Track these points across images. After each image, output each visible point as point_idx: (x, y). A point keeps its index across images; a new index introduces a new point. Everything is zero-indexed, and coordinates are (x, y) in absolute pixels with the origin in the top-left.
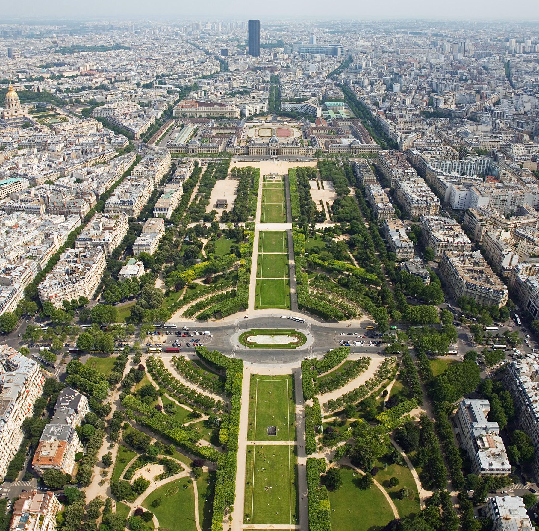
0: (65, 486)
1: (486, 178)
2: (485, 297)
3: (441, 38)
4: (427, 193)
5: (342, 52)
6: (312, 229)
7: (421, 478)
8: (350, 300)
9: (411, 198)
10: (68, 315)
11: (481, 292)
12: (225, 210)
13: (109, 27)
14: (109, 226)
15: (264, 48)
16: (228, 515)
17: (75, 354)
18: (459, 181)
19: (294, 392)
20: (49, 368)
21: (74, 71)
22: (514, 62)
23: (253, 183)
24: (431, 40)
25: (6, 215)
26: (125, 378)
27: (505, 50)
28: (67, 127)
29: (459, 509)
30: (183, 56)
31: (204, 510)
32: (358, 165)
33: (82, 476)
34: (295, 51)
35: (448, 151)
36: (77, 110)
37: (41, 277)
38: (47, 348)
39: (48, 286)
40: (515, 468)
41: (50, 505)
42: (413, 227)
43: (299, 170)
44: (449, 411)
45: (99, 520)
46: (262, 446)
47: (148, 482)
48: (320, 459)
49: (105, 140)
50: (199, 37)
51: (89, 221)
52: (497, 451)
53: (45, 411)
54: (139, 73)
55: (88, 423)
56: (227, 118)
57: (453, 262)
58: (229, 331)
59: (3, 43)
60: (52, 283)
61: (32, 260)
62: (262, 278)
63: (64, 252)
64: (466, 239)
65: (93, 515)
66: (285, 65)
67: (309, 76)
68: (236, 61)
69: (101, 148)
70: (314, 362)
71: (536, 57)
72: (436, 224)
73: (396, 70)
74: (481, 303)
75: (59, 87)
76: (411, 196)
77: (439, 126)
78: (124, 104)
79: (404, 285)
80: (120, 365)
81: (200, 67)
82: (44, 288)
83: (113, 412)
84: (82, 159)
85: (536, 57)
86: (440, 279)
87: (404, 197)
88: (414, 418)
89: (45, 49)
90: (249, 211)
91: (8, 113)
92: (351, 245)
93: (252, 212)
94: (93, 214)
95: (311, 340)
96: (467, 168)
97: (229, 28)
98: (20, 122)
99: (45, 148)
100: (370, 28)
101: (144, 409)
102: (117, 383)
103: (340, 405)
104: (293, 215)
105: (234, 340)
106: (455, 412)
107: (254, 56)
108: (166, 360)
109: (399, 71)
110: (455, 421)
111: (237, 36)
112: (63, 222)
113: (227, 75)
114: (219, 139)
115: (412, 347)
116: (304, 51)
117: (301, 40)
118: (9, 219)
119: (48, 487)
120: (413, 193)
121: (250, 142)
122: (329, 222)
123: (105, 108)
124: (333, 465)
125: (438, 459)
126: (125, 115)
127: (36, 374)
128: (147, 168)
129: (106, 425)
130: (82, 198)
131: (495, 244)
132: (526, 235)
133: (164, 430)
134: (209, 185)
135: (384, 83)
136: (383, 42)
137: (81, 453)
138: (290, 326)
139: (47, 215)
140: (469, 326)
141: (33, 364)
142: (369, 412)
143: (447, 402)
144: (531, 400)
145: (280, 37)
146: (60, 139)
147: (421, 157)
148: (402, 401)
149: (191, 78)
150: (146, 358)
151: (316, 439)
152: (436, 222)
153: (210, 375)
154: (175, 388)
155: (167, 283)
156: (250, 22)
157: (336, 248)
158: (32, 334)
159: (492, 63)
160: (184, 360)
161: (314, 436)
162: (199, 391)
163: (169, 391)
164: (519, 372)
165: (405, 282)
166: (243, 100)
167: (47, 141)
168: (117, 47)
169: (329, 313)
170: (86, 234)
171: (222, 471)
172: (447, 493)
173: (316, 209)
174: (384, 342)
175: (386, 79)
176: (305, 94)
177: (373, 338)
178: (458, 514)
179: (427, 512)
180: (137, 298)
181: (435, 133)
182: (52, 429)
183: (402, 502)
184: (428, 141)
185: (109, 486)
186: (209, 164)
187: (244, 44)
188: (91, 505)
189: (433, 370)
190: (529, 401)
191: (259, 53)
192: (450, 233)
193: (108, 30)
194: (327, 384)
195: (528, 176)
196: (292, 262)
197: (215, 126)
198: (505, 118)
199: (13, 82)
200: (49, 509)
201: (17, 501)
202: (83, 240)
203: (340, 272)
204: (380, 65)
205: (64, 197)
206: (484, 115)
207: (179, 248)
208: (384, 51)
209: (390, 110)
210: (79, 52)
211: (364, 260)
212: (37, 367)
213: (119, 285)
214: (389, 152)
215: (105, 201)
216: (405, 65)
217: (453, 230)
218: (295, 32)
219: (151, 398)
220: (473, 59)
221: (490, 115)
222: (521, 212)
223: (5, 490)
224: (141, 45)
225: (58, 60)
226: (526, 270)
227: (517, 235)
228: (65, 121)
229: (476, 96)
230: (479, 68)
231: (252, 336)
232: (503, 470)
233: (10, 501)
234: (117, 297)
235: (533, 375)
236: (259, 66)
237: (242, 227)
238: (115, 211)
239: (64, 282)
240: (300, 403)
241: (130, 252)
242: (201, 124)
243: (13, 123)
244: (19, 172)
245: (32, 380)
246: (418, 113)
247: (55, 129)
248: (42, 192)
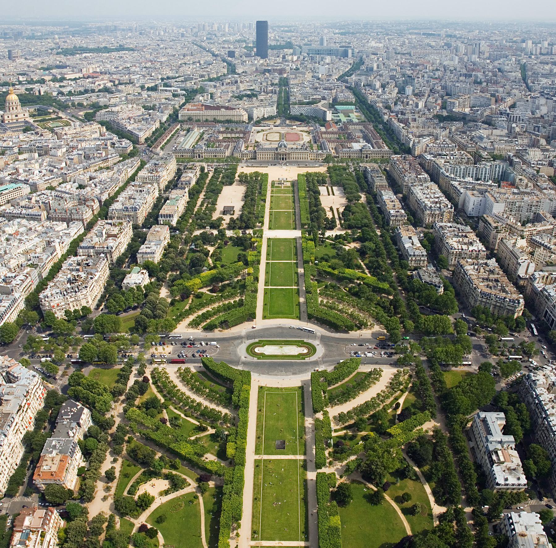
0: (67, 501)
1: (502, 184)
2: (500, 307)
3: (454, 39)
4: (441, 199)
5: (353, 53)
6: (322, 236)
7: (434, 493)
8: (361, 310)
9: (424, 204)
10: (70, 325)
11: (497, 301)
12: (232, 216)
13: (113, 28)
14: (113, 233)
15: (272, 49)
16: (235, 532)
17: (77, 366)
18: (474, 187)
19: (303, 405)
20: (51, 380)
21: (76, 73)
23: (261, 188)
24: (445, 41)
25: (7, 222)
26: (129, 390)
27: (521, 52)
28: (69, 131)
29: (474, 525)
30: (189, 58)
31: (211, 526)
32: (370, 170)
33: (84, 492)
34: (304, 52)
35: (462, 156)
36: (79, 113)
37: (42, 285)
38: (49, 359)
39: (49, 295)
40: (531, 483)
41: (52, 521)
42: (426, 235)
43: (308, 175)
44: (463, 424)
45: (102, 537)
46: (270, 461)
48: (331, 474)
49: (109, 144)
50: (205, 38)
51: (92, 228)
52: (513, 466)
53: (46, 424)
54: (144, 76)
55: (91, 436)
56: (234, 122)
57: (467, 270)
58: (236, 342)
59: (3, 44)
60: (54, 292)
61: (33, 269)
62: (270, 287)
63: (66, 260)
64: (481, 247)
65: (96, 532)
66: (294, 67)
67: (319, 79)
68: (243, 63)
69: (104, 152)
70: (323, 374)
71: (553, 59)
72: (450, 232)
74: (496, 313)
75: (61, 89)
76: (424, 202)
77: (453, 130)
78: (127, 107)
79: (417, 294)
80: (123, 377)
81: (206, 70)
82: (45, 297)
83: (116, 425)
84: (84, 164)
85: (553, 59)
86: (454, 288)
87: (416, 203)
88: (427, 431)
89: (47, 51)
90: (257, 218)
91: (8, 117)
92: (362, 253)
93: (260, 219)
94: (96, 221)
95: (321, 350)
96: (482, 174)
97: (236, 28)
98: (21, 126)
99: (46, 153)
100: (382, 29)
101: (149, 422)
102: (121, 395)
103: (351, 418)
104: (303, 222)
105: (241, 351)
106: (469, 425)
107: (262, 58)
108: (172, 371)
109: (412, 74)
110: (470, 434)
111: (245, 37)
112: (65, 229)
113: (234, 77)
114: (226, 143)
115: (425, 358)
116: (314, 52)
117: (311, 41)
118: (9, 226)
119: (50, 503)
120: (426, 200)
121: (257, 146)
122: (339, 229)
123: (109, 111)
124: (343, 480)
125: (451, 474)
126: (129, 118)
127: (37, 386)
128: (152, 173)
129: (109, 439)
130: (85, 204)
131: (511, 252)
132: (543, 242)
133: (169, 444)
134: (216, 191)
135: (396, 86)
136: (395, 43)
137: (84, 467)
138: (299, 337)
139: (48, 222)
140: (484, 337)
141: (34, 376)
142: (381, 425)
143: (461, 415)
144: (548, 412)
145: (289, 38)
146: (62, 143)
147: (434, 162)
148: (414, 414)
149: (197, 81)
150: (151, 370)
151: (326, 453)
152: (450, 229)
153: (217, 387)
154: (181, 401)
155: (172, 293)
156: (258, 23)
157: (347, 256)
158: (33, 344)
159: (508, 65)
160: (190, 372)
161: (324, 449)
162: (206, 403)
163: (174, 404)
164: (535, 384)
165: (417, 291)
166: (250, 103)
167: (48, 146)
168: (121, 48)
169: (340, 323)
170: (89, 242)
171: (229, 486)
172: (461, 509)
173: (326, 215)
174: (396, 353)
175: (398, 81)
176: (314, 97)
177: (384, 348)
178: (473, 530)
179: (440, 529)
180: (141, 308)
181: (449, 137)
182: (54, 443)
183: (414, 518)
184: (442, 145)
185: (112, 501)
186: (215, 169)
187: (252, 45)
188: (93, 521)
189: (447, 382)
190: (546, 413)
191: (267, 54)
192: (465, 241)
193: (112, 31)
194: (337, 396)
195: (545, 182)
196: (301, 271)
197: (222, 130)
198: (521, 122)
199: (14, 85)
200: (51, 525)
201: (17, 517)
202: (86, 248)
203: (351, 281)
204: (392, 67)
205: (66, 203)
207: (185, 256)
208: (396, 53)
209: (403, 114)
210: (81, 53)
211: (375, 268)
212: (38, 379)
213: (123, 294)
214: (401, 157)
215: (108, 208)
216: (418, 68)
217: (467, 237)
218: (304, 33)
219: (155, 411)
220: (488, 61)
221: (505, 119)
222: (537, 219)
223: (6, 505)
224: (145, 47)
225: (60, 62)
226: (543, 279)
227: (533, 243)
228: (67, 125)
229: (491, 99)
230: (495, 70)
232: (519, 485)
233: (11, 517)
234: (121, 306)
236: (267, 68)
237: (249, 234)
238: (118, 218)
239: (66, 291)
240: (309, 416)
241: (134, 260)
242: (208, 128)
243: (13, 127)
244: (20, 178)
246: (431, 117)
247: (56, 134)
248: (43, 198)
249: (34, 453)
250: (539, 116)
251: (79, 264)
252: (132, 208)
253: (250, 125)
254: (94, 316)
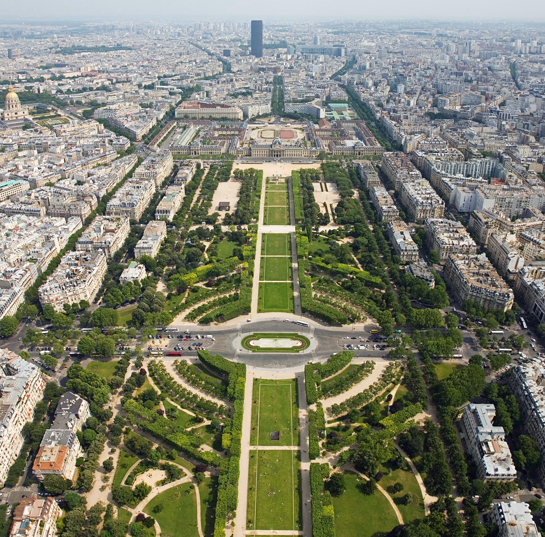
0: (66, 491)
1: (492, 180)
2: (490, 300)
3: (445, 38)
4: (432, 195)
5: (346, 52)
6: (315, 231)
7: (426, 483)
8: (353, 303)
9: (415, 200)
10: (69, 319)
11: (487, 295)
12: (228, 212)
13: (110, 27)
14: (111, 228)
15: (267, 48)
16: (230, 521)
17: (76, 358)
18: (464, 183)
19: (297, 397)
20: (50, 372)
21: (75, 72)
22: (520, 63)
23: (255, 185)
24: (436, 41)
25: (7, 217)
26: (126, 382)
27: (511, 51)
28: (68, 129)
29: (464, 515)
30: (185, 57)
31: (206, 516)
32: (362, 166)
33: (83, 482)
34: (298, 51)
35: (453, 152)
36: (78, 111)
37: (41, 280)
38: (48, 352)
39: (48, 289)
40: (521, 474)
41: (51, 511)
42: (417, 230)
43: (302, 172)
44: (454, 416)
45: (100, 526)
46: (264, 451)
47: (150, 487)
48: (324, 465)
49: (107, 141)
50: (201, 37)
51: (90, 223)
52: (503, 457)
53: (45, 416)
54: (141, 74)
55: (89, 428)
56: (229, 119)
57: (458, 265)
58: (232, 335)
60: (53, 286)
61: (33, 263)
62: (265, 281)
63: (64, 255)
64: (471, 242)
65: (94, 521)
66: (289, 66)
67: (312, 77)
68: (238, 61)
69: (102, 149)
70: (317, 366)
71: (542, 58)
72: (441, 227)
73: (401, 71)
75: (60, 88)
76: (415, 198)
77: (444, 127)
78: (125, 105)
79: (409, 288)
80: (121, 369)
81: (202, 68)
82: (44, 291)
83: (114, 417)
84: (83, 161)
85: (542, 58)
86: (445, 282)
87: (408, 199)
88: (418, 423)
89: (46, 50)
90: (252, 213)
91: (8, 115)
92: (355, 248)
93: (255, 215)
94: (94, 217)
95: (314, 343)
96: (472, 170)
97: (231, 28)
98: (20, 124)
99: (45, 150)
100: (374, 28)
101: (146, 414)
102: (119, 387)
103: (344, 409)
104: (297, 217)
105: (237, 344)
106: (460, 416)
107: (257, 56)
108: (168, 364)
109: (404, 72)
110: (460, 426)
111: (240, 37)
112: (64, 225)
113: (229, 76)
114: (222, 141)
115: (416, 351)
116: (308, 51)
117: (305, 40)
119: (49, 492)
120: (418, 196)
121: (252, 143)
122: (332, 225)
123: (107, 109)
124: (336, 470)
125: (442, 464)
126: (127, 116)
127: (36, 378)
128: (149, 170)
129: (107, 430)
130: (83, 200)
131: (501, 247)
132: (532, 237)
133: (165, 435)
134: (212, 188)
135: (388, 84)
136: (388, 42)
137: (82, 458)
138: (293, 330)
139: (47, 218)
140: (474, 330)
141: (33, 369)
142: (373, 417)
143: (452, 407)
144: (537, 404)
145: (283, 37)
146: (61, 140)
147: (426, 158)
148: (406, 405)
149: (193, 79)
150: (148, 362)
151: (320, 444)
152: (441, 224)
153: (212, 380)
154: (177, 393)
155: (169, 287)
156: (253, 22)
157: (340, 251)
158: (33, 338)
159: (498, 64)
160: (186, 364)
161: (317, 440)
162: (202, 395)
163: (171, 396)
164: (525, 377)
165: (409, 285)
166: (245, 101)
167: (47, 143)
168: (119, 47)
169: (333, 317)
170: (87, 237)
171: (225, 476)
172: (452, 499)
173: (319, 211)
174: (388, 346)
175: (390, 80)
176: (308, 95)
177: (377, 341)
178: (463, 520)
179: (431, 518)
180: (139, 302)
181: (440, 135)
182: (53, 434)
183: (406, 508)
184: (433, 142)
185: (110, 491)
186: (211, 166)
187: (247, 44)
188: (92, 511)
189: (438, 374)
190: (535, 405)
191: (262, 53)
192: (455, 236)
193: (109, 31)
194: (331, 388)
195: (534, 178)
196: (295, 265)
197: (217, 127)
198: (511, 119)
199: (13, 83)
201: (17, 507)
202: (84, 243)
203: (344, 275)
204: (384, 65)
205: (64, 199)
206: (490, 117)
207: (181, 251)
208: (388, 52)
209: (395, 111)
210: (80, 52)
211: (368, 263)
212: (37, 371)
213: (121, 288)
215: (106, 204)
216: (410, 66)
217: (458, 232)
218: (298, 32)
219: (152, 403)
220: (479, 60)
221: (495, 117)
222: (527, 214)
223: (6, 495)
224: (142, 46)
225: (59, 61)
226: (532, 273)
227: (522, 238)
228: (65, 123)
229: (481, 97)
230: (485, 68)
231: (254, 339)
232: (509, 475)
233: (10, 507)
234: (118, 300)
235: (539, 380)
236: (261, 67)
237: (244, 229)
238: (116, 214)
239: (65, 285)
240: (303, 408)
241: (131, 255)
242: (203, 125)
243: (13, 125)
244: (19, 174)
245: (33, 384)
246: (422, 114)
247: (55, 131)
248: (42, 194)
249: (34, 444)
250: (528, 113)
251: (77, 259)
252: (130, 203)
253: (245, 123)
254: (92, 309)
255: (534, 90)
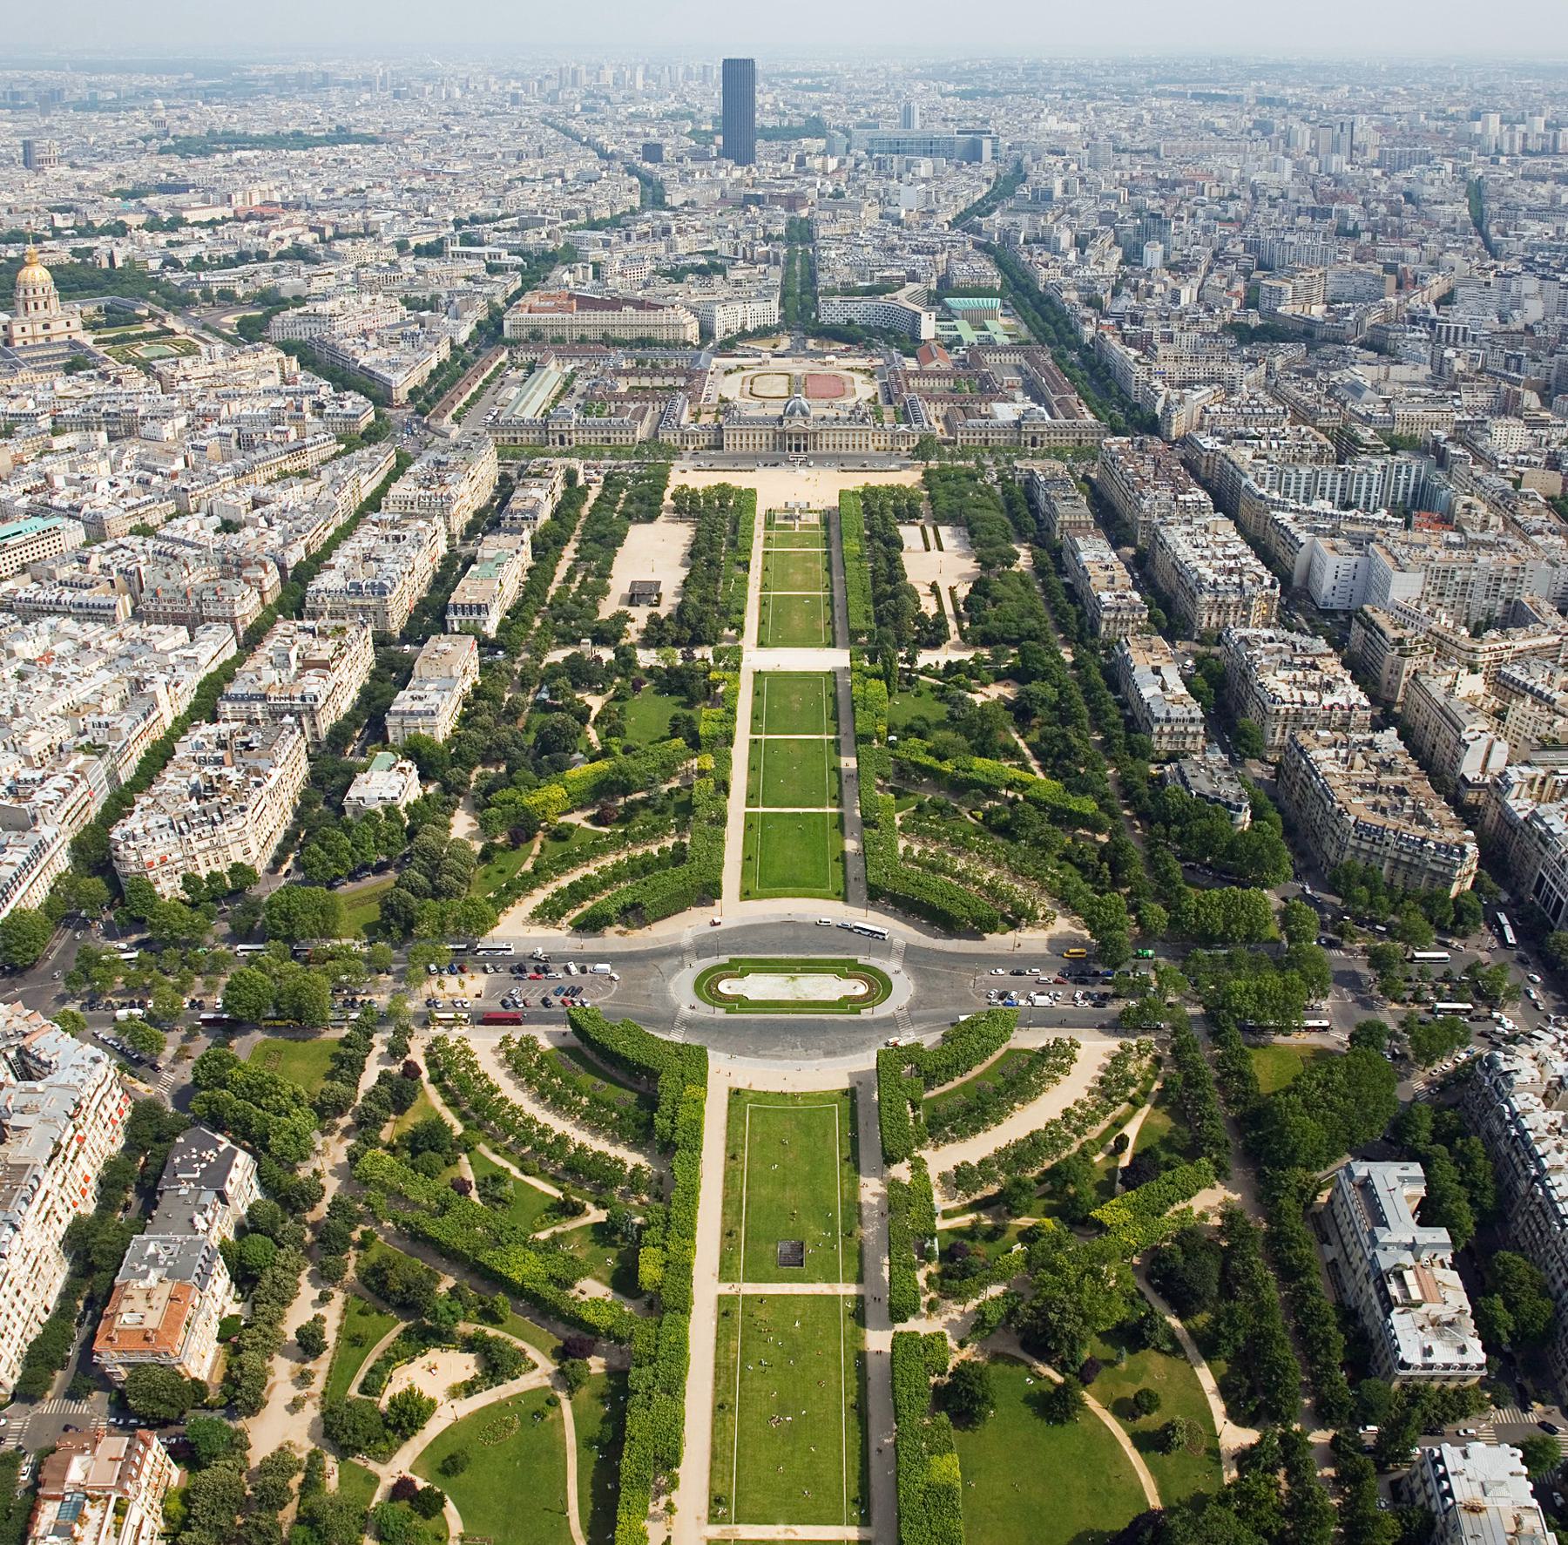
0: (190, 1413)
1: (1415, 519)
2: (1409, 864)
3: (1282, 110)
4: (1243, 561)
5: (994, 151)
6: (907, 666)
7: (1224, 1390)
8: (1017, 873)
9: (1195, 576)
10: (198, 917)
11: (1400, 850)
12: (655, 610)
13: (318, 78)
14: (319, 657)
15: (767, 139)
16: (663, 1500)
17: (218, 1031)
18: (1336, 527)
19: (854, 1141)
20: (143, 1070)
21: (214, 206)
23: (735, 531)
24: (1255, 117)
25: (19, 625)
26: (364, 1099)
27: (1470, 145)
28: (196, 370)
29: (1336, 1481)
30: (532, 163)
31: (594, 1484)
32: (1042, 479)
33: (238, 1386)
34: (858, 148)
35: (1303, 439)
36: (223, 320)
37: (119, 805)
38: (137, 1011)
39: (139, 832)
40: (1498, 1363)
41: (146, 1469)
42: (1200, 662)
43: (869, 494)
44: (1305, 1196)
45: (288, 1514)
46: (761, 1299)
48: (932, 1337)
49: (306, 406)
50: (578, 108)
51: (260, 642)
52: (1447, 1314)
53: (130, 1196)
54: (405, 214)
55: (255, 1230)
56: (659, 344)
57: (1317, 762)
58: (666, 964)
60: (151, 823)
61: (94, 757)
62: (761, 810)
63: (185, 732)
64: (1356, 695)
65: (271, 1499)
66: (831, 190)
67: (899, 222)
68: (686, 176)
69: (293, 430)
70: (912, 1053)
71: (1559, 166)
72: (1269, 653)
73: (1153, 205)
74: (1398, 882)
75: (173, 252)
76: (1195, 570)
77: (1278, 367)
78: (359, 302)
79: (1176, 829)
80: (348, 1063)
81: (582, 196)
82: (127, 839)
83: (328, 1199)
84: (238, 462)
85: (1559, 166)
86: (1281, 811)
88: (1203, 1216)
89: (132, 143)
90: (724, 614)
91: (23, 330)
92: (1021, 712)
93: (735, 618)
94: (272, 623)
95: (904, 988)
96: (1359, 490)
97: (665, 80)
98: (58, 356)
99: (131, 432)
100: (1077, 81)
101: (420, 1190)
102: (342, 1113)
103: (989, 1178)
104: (853, 625)
105: (681, 990)
106: (1323, 1198)
107: (740, 162)
108: (484, 1046)
109: (1162, 208)
110: (1324, 1224)
111: (690, 106)
112: (183, 647)
113: (659, 218)
114: (638, 404)
115: (1198, 1010)
116: (886, 148)
117: (876, 116)
118: (25, 637)
119: (140, 1417)
120: (1202, 563)
121: (726, 412)
122: (956, 647)
123: (307, 314)
124: (967, 1353)
125: (1273, 1335)
126: (365, 334)
127: (104, 1089)
128: (428, 488)
129: (309, 1236)
130: (239, 575)
131: (1441, 709)
132: (1531, 683)
133: (476, 1250)
134: (609, 540)
135: (1116, 243)
136: (1115, 121)
137: (237, 1317)
138: (843, 950)
139: (136, 627)
140: (1364, 950)
141: (96, 1060)
142: (1074, 1199)
143: (1300, 1171)
145: (815, 108)
146: (176, 403)
147: (1225, 456)
148: (1169, 1167)
149: (555, 227)
150: (426, 1042)
151: (921, 1276)
152: (1269, 645)
153: (611, 1092)
154: (509, 1130)
155: (485, 825)
156: (728, 64)
157: (979, 721)
158: (94, 971)
159: (1432, 183)
160: (535, 1048)
161: (913, 1267)
162: (580, 1137)
163: (492, 1138)
164: (1510, 1083)
165: (1177, 821)
166: (706, 290)
167: (136, 411)
168: (341, 136)
169: (958, 911)
171: (647, 1371)
172: (1301, 1435)
173: (919, 608)
174: (1117, 996)
175: (1122, 229)
176: (887, 274)
177: (1084, 982)
178: (1333, 1495)
179: (1241, 1491)
180: (399, 868)
181: (1266, 387)
182: (151, 1249)
183: (1169, 1461)
184: (1246, 410)
185: (316, 1413)
186: (607, 478)
187: (710, 128)
188: (264, 1470)
189: (1261, 1077)
190: (1539, 1166)
191: (754, 153)
192: (1310, 679)
193: (315, 88)
194: (952, 1117)
195: (1537, 512)
196: (849, 763)
197: (625, 365)
198: (1469, 343)
199: (38, 239)
200: (143, 1481)
201: (48, 1458)
202: (243, 699)
203: (990, 791)
204: (1105, 188)
205: (185, 573)
206: (1409, 335)
207: (522, 722)
208: (1116, 150)
210: (230, 151)
211: (1058, 757)
212: (107, 1067)
213: (347, 828)
215: (305, 586)
216: (1179, 191)
217: (1317, 668)
218: (857, 92)
219: (438, 1159)
220: (1377, 172)
221: (1424, 335)
222: (1515, 616)
223: (16, 1425)
224: (409, 131)
225: (169, 175)
226: (1531, 786)
227: (1503, 685)
228: (188, 353)
229: (1383, 280)
230: (1395, 197)
231: (732, 976)
232: (1464, 1367)
233: (30, 1459)
234: (340, 863)
236: (752, 192)
237: (703, 659)
238: (334, 615)
239: (186, 820)
240: (872, 1173)
241: (377, 734)
242: (585, 361)
243: (37, 359)
244: (55, 501)
245: (94, 1105)
246: (1215, 329)
247: (159, 377)
248: (122, 559)
249: (96, 1276)
251: (222, 745)
252: (373, 585)
253: (704, 353)
254: (266, 890)
255: (1538, 259)
